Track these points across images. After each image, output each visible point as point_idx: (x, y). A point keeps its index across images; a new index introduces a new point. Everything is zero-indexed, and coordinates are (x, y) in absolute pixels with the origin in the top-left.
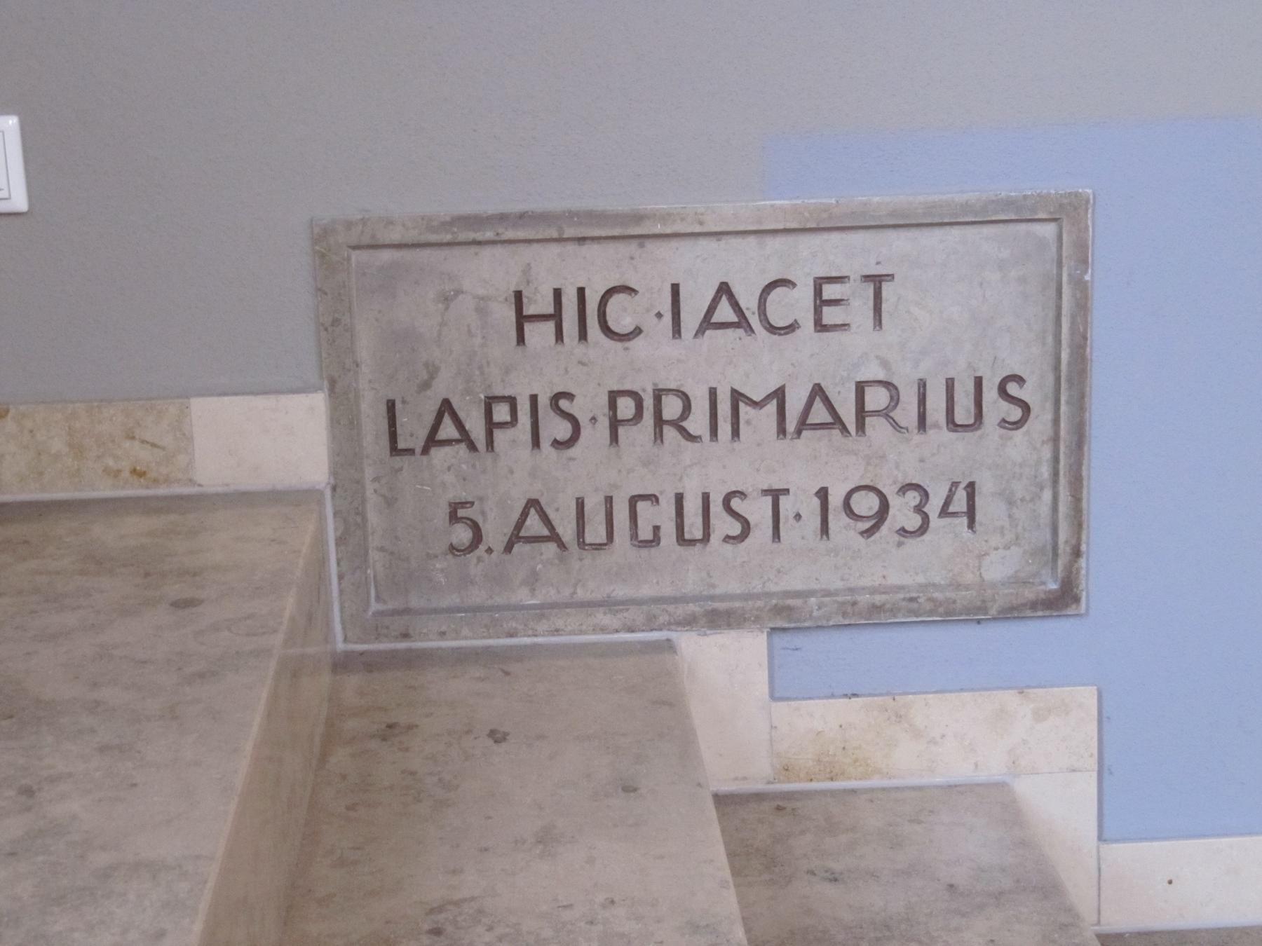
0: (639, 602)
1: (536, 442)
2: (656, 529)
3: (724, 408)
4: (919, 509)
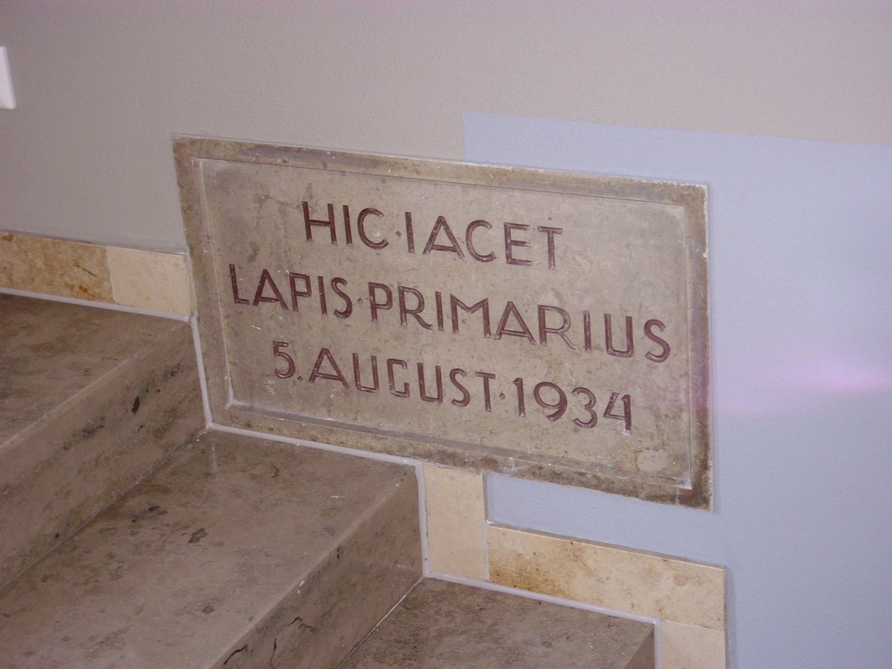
0: (394, 435)
1: (324, 310)
2: (406, 385)
3: (447, 308)
4: (589, 407)
